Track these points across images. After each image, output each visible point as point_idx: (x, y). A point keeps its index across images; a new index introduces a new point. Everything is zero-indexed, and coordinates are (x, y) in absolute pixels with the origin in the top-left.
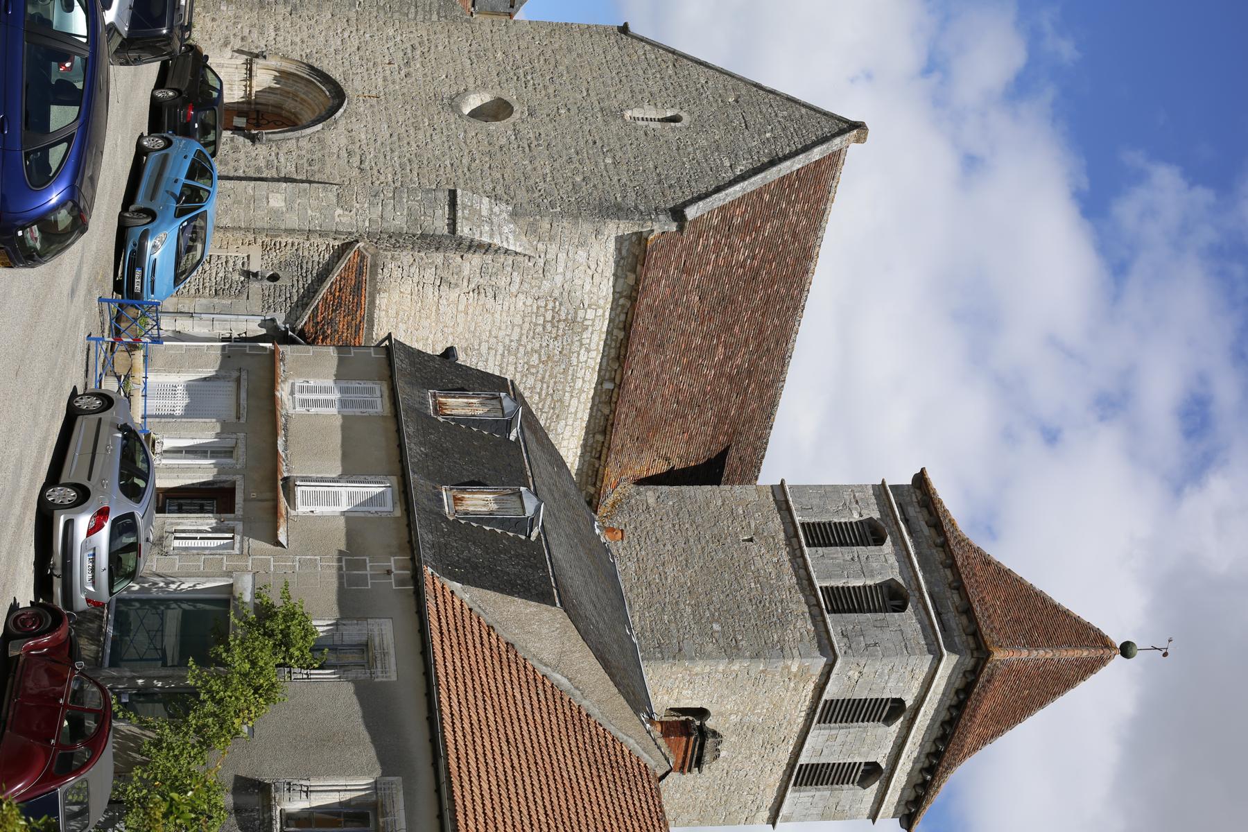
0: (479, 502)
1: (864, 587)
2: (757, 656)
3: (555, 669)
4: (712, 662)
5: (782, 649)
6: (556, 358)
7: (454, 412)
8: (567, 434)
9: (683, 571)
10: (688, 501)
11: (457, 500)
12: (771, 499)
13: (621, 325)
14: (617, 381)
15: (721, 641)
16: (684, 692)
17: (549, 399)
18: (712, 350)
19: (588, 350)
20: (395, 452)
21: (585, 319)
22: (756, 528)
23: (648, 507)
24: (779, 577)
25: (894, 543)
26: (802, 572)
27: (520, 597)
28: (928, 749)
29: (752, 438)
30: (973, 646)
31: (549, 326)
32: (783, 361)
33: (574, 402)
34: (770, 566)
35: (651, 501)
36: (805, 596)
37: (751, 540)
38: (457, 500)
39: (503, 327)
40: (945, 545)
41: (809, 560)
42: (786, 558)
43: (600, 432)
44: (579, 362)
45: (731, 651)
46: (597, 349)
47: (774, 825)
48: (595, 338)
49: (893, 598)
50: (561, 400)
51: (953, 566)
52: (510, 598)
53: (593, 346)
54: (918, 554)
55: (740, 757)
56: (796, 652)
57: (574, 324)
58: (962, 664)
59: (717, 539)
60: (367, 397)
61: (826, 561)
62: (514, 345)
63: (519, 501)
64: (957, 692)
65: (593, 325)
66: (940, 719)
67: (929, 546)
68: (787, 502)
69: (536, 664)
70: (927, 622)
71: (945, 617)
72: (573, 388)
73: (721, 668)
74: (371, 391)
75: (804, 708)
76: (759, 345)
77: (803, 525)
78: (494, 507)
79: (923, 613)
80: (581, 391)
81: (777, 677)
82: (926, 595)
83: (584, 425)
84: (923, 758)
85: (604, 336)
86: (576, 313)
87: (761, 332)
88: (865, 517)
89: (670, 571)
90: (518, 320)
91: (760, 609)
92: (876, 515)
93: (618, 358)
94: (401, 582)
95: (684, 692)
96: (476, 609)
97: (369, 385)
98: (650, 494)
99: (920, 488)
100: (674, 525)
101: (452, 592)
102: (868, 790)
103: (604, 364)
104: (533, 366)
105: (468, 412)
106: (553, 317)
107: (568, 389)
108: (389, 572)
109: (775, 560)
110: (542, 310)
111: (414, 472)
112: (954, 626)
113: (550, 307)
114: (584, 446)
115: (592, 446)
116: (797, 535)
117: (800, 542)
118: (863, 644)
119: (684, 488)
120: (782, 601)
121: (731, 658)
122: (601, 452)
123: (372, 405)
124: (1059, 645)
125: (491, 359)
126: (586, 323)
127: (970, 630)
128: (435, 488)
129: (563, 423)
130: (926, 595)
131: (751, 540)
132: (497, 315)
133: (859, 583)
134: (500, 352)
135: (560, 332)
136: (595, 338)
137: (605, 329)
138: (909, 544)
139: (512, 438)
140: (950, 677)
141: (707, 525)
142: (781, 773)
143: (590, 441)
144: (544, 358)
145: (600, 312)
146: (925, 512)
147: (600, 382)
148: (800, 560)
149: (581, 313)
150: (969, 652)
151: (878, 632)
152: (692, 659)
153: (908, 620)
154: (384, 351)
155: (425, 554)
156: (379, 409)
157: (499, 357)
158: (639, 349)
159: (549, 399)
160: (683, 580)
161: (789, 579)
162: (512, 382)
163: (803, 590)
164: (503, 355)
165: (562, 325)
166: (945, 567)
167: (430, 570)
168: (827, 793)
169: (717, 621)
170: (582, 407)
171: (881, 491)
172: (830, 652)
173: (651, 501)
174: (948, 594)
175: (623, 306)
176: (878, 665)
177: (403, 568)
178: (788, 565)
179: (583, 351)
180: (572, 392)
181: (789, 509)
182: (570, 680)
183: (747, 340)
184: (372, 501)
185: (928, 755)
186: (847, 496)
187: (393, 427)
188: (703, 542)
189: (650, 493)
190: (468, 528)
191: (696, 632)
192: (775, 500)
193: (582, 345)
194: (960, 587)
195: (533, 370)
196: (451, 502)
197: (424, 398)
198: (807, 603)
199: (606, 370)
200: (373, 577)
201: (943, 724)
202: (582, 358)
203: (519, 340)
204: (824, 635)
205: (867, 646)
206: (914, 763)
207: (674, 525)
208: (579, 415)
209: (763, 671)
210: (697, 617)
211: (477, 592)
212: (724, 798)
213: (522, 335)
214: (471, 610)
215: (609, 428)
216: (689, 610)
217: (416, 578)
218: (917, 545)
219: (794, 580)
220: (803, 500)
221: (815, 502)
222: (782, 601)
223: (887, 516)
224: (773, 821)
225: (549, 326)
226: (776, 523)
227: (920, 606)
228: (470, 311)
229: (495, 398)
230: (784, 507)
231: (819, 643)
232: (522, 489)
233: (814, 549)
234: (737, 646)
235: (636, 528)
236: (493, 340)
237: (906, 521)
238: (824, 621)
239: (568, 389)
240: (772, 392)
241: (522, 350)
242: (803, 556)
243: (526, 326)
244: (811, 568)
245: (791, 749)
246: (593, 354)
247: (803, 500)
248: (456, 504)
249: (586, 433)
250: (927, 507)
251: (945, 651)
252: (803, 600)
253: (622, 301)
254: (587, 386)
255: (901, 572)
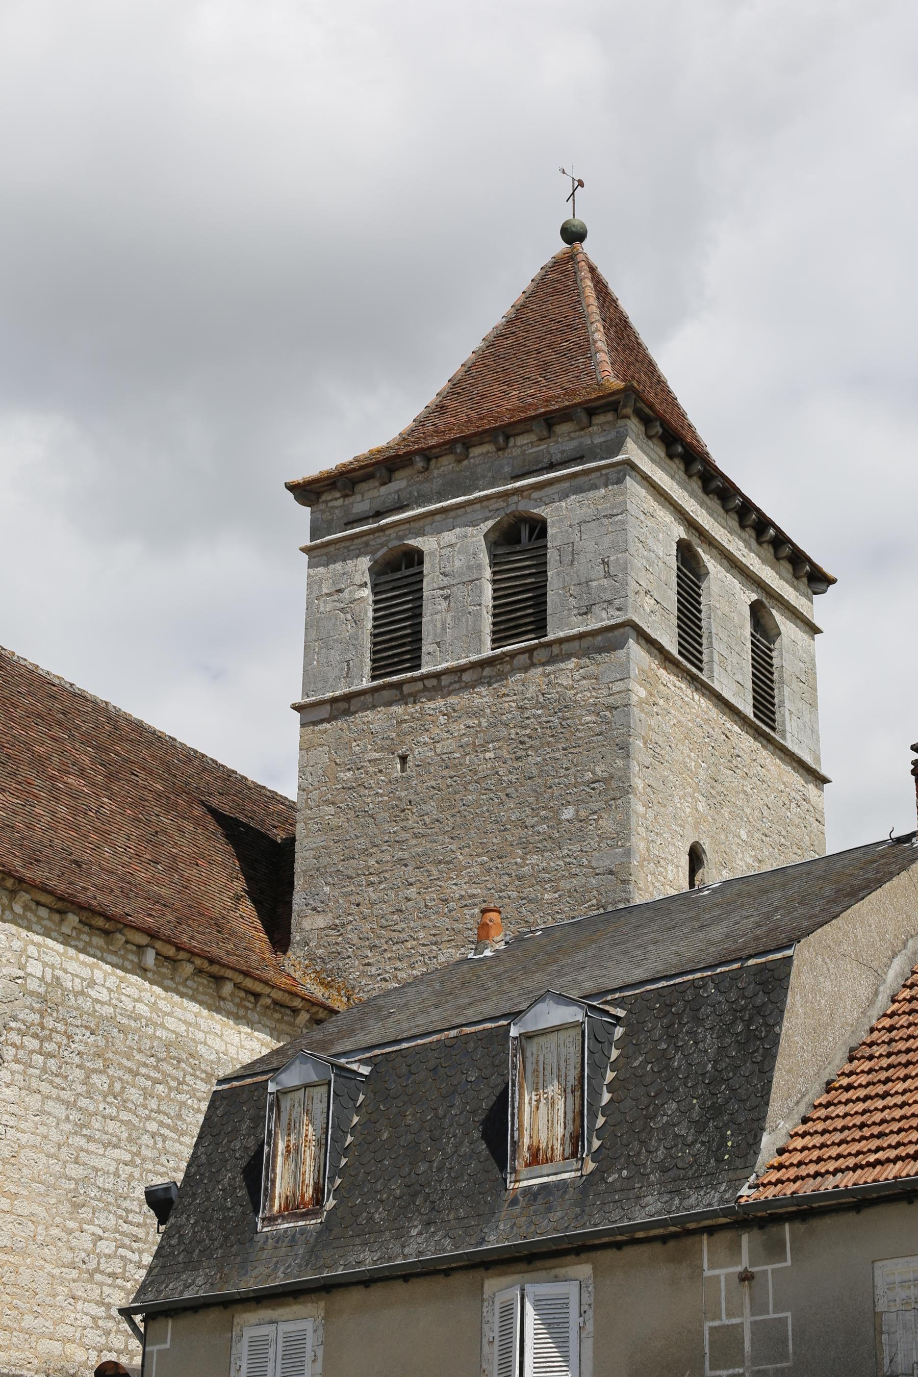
0: (541, 1118)
1: (494, 582)
2: (624, 749)
3: (880, 977)
4: (633, 820)
6: (102, 1043)
7: (309, 1179)
8: (218, 1044)
9: (459, 870)
10: (325, 860)
11: (536, 1158)
12: (326, 726)
13: (56, 917)
14: (143, 940)
15: (594, 806)
16: (670, 876)
17: (165, 1066)
18: (74, 795)
19: (92, 983)
20: (420, 1286)
21: (42, 979)
22: (382, 749)
23: (335, 927)
25: (421, 533)
26: (467, 677)
27: (779, 1023)
28: (734, 524)
29: (191, 771)
30: (610, 417)
31: (50, 1047)
32: (80, 697)
33: (170, 1023)
34: (453, 727)
35: (321, 921)
36: (513, 671)
37: (403, 759)
38: (536, 1158)
39: (42, 1130)
40: (428, 455)
41: (445, 665)
42: (440, 702)
43: (218, 989)
44: (109, 1003)
45: (615, 790)
46: (92, 967)
47: (825, 780)
48: (72, 966)
49: (520, 541)
50: (168, 1046)
51: (467, 443)
52: (783, 1042)
53: (85, 973)
54: (441, 497)
55: (748, 811)
56: (616, 688)
57: (50, 999)
58: (638, 436)
59: (399, 812)
60: (275, 1352)
61: (448, 638)
62: (74, 1116)
63: (542, 1040)
64: (671, 456)
65: (53, 967)
66: (699, 491)
67: (426, 480)
68: (334, 700)
69: (876, 1012)
70: (566, 485)
71: (557, 458)
72: (149, 1022)
73: (641, 809)
74: (259, 1347)
75: (689, 692)
76: (60, 724)
77: (374, 678)
78: (553, 1089)
79: (549, 490)
80: (154, 1007)
81: (653, 722)
83: (205, 1012)
84: (745, 535)
85: (72, 952)
86: (32, 993)
87: (39, 716)
88: (367, 578)
89: (457, 888)
90: (34, 1101)
91: (537, 743)
92: (365, 562)
93: (106, 933)
94: (775, 1250)
95: (670, 876)
96: (802, 1110)
97: (242, 1349)
98: (307, 922)
99: (319, 494)
100: (371, 884)
101: (781, 1152)
102: (782, 627)
103: (115, 959)
104: (111, 1086)
105: (309, 1154)
106: (35, 1036)
107: (150, 1031)
108: (746, 1277)
109: (442, 719)
110: (21, 1053)
111: (483, 1241)
112: (573, 444)
113: (17, 1039)
114: (237, 1018)
115: (239, 1006)
116: (398, 685)
117: (413, 680)
118: (605, 582)
119: (298, 867)
120: (522, 708)
121: (627, 790)
122: (248, 992)
123: (294, 1344)
124: (583, 316)
125: (94, 1161)
126: (48, 978)
127: (584, 417)
128: (514, 1202)
129: (202, 1049)
131: (403, 759)
132: (24, 1138)
133: (488, 590)
134: (83, 1142)
135: (60, 1027)
136: (72, 966)
137: (60, 948)
139: (365, 1070)
140: (652, 460)
141: (372, 830)
142: (765, 753)
143: (230, 1006)
144: (99, 1064)
145: (32, 950)
146: (363, 486)
147: (142, 971)
148: (445, 680)
149: (33, 985)
150: (621, 422)
151: (582, 558)
152: (628, 853)
153: (562, 516)
154: (157, 1325)
155: (705, 1201)
156: (308, 1325)
157: (92, 1147)
159: (165, 1066)
160: (477, 869)
161: (482, 697)
162: (220, 1082)
163: (502, 677)
164: (89, 1139)
165: (49, 1023)
166: (467, 457)
167: (744, 1191)
168: (787, 691)
169: (557, 812)
170: (178, 1012)
171: (318, 554)
172: (617, 632)
173: (321, 921)
174: (516, 452)
175: (26, 907)
176: (638, 563)
177: (736, 1247)
179: (92, 993)
180: (155, 1024)
181: (348, 698)
182: (895, 955)
183: (55, 739)
184: (554, 1326)
185: (743, 526)
186: (327, 606)
187: (356, 1295)
188: (404, 835)
189: (306, 924)
190: (614, 1136)
191: (577, 847)
192: (328, 720)
193: (82, 993)
194: (503, 434)
195: (118, 1086)
196: (546, 1168)
197: (279, 1238)
198: (526, 669)
199: (124, 958)
200: (758, 1307)
201: (706, 491)
202: (104, 996)
203: (68, 1105)
204: (585, 643)
205: (608, 575)
206: (751, 550)
207: (371, 884)
208: (191, 1018)
209: (645, 743)
210: (549, 844)
211: (776, 1106)
212: (795, 850)
213: (58, 1099)
214: (805, 1120)
215: (215, 969)
216: (534, 859)
217: (763, 1219)
219: (483, 690)
220: (332, 675)
221: (335, 656)
222: (522, 708)
223: (367, 544)
224: (821, 780)
225: (50, 1047)
226: (375, 719)
227: (535, 495)
228: (13, 1188)
229: (277, 1103)
230: (342, 705)
231: (600, 650)
232: (514, 1032)
233: (425, 658)
234: (605, 781)
235: (372, 948)
236: (64, 1153)
237: (379, 515)
238: (561, 641)
239: (150, 1031)
240: (123, 724)
241: (83, 1102)
242: (437, 675)
243: (45, 1087)
244: (463, 661)
245: (736, 728)
246: (98, 975)
247: (332, 675)
248: (550, 1160)
249: (218, 1011)
251: (620, 457)
253: (18, 909)
254: (146, 996)
255: (474, 524)
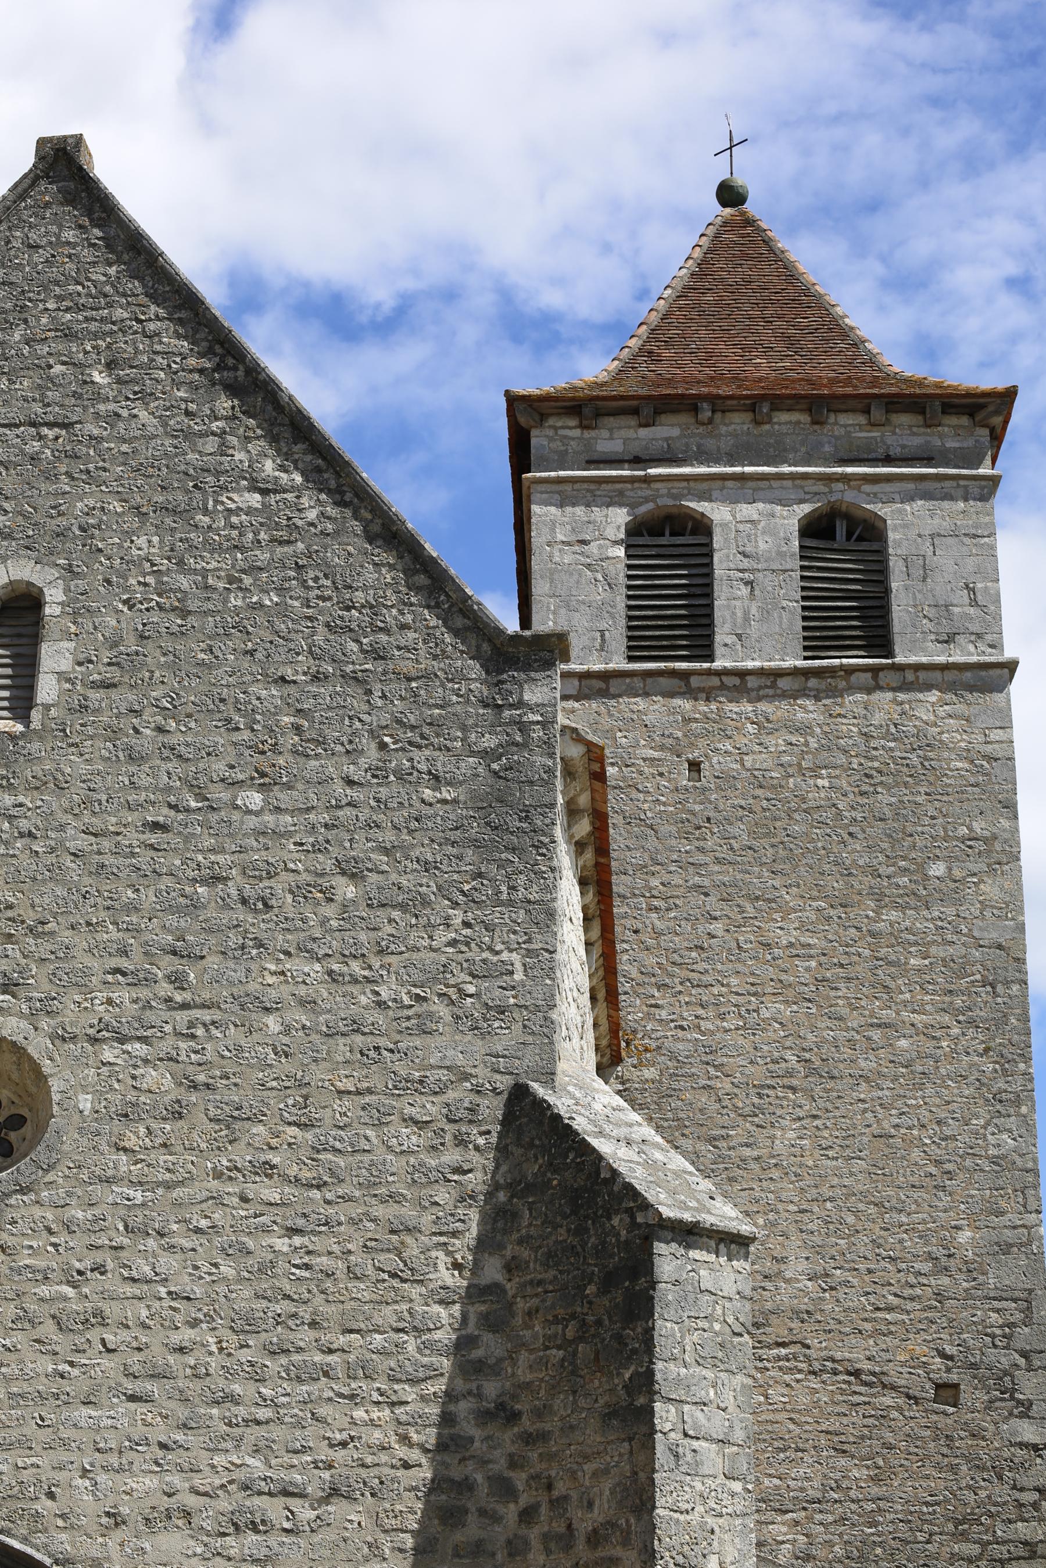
5: (991, 759)
24: (804, 729)
26: (783, 683)
30: (965, 421)
37: (695, 766)
70: (911, 486)
71: (896, 451)
77: (631, 659)
82: (850, 470)
92: (619, 517)
112: (917, 441)
130: (850, 470)
131: (695, 766)
138: (703, 470)
158: (719, 483)
163: (834, 693)
178: (763, 706)
188: (700, 858)
191: (950, 911)
192: (577, 699)
198: (869, 691)
204: (950, 676)
218: (703, 456)
227: (867, 488)
231: (971, 688)
250: (599, 414)
252: (859, 697)
